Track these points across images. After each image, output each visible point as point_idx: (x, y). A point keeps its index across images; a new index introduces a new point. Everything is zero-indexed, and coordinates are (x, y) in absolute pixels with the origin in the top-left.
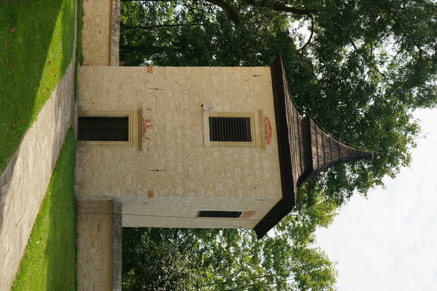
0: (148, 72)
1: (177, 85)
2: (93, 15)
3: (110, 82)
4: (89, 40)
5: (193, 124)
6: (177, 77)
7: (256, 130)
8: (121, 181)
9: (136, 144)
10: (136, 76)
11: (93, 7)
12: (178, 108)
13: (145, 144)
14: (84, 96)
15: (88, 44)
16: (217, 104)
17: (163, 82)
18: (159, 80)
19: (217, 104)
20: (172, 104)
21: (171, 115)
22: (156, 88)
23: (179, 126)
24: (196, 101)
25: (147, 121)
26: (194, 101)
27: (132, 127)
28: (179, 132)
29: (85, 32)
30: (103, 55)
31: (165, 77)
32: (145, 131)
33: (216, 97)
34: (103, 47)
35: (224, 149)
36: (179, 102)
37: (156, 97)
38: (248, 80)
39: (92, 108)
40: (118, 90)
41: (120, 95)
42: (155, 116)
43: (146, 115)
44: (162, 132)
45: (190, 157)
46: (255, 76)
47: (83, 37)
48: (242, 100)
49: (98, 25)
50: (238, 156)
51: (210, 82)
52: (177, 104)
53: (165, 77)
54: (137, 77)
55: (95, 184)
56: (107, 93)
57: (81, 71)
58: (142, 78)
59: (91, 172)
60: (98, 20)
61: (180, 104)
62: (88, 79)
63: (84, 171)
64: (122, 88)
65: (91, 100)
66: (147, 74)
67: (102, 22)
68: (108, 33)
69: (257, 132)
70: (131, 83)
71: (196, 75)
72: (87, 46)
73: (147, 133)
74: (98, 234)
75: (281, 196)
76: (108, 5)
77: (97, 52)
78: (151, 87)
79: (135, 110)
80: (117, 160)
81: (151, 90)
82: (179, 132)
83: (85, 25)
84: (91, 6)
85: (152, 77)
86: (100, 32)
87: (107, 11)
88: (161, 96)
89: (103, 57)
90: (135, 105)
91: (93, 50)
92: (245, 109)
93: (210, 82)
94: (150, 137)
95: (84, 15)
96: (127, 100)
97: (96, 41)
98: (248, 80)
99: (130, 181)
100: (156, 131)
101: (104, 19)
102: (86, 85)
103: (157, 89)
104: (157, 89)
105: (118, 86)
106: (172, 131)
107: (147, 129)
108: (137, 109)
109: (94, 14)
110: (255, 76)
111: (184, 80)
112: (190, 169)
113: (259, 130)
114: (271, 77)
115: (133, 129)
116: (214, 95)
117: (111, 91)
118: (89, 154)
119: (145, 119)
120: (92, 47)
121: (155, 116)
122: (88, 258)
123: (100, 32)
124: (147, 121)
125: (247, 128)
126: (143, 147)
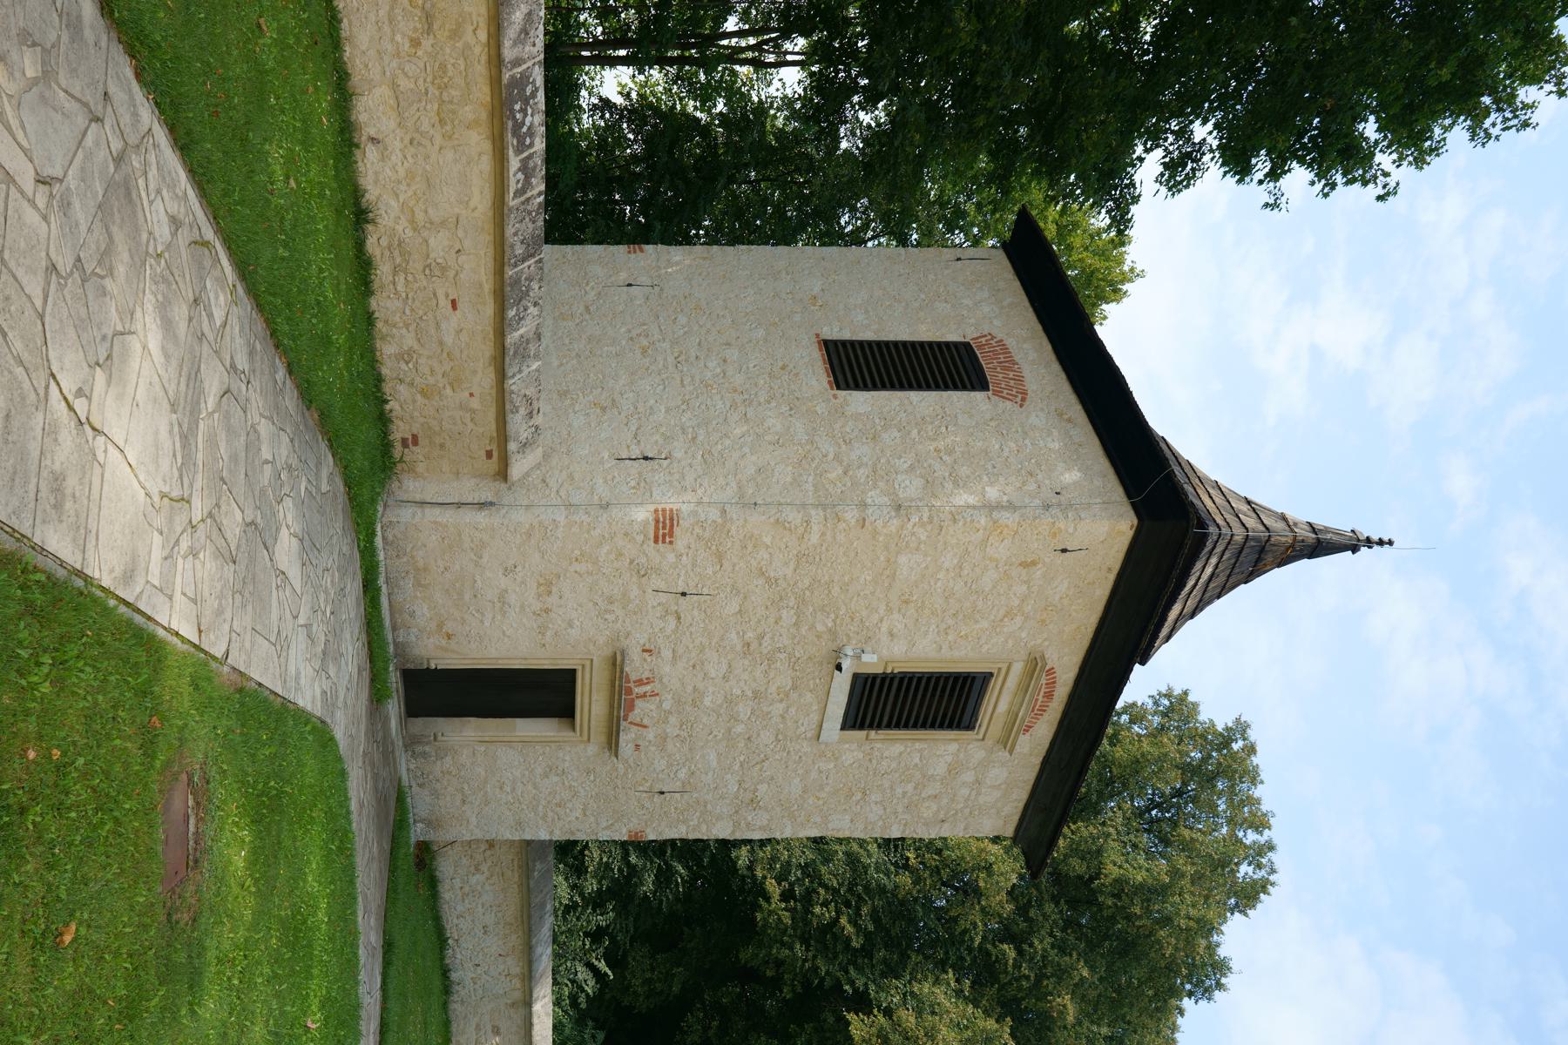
0: (656, 541)
1: (761, 581)
2: (412, 221)
3: (506, 572)
4: (409, 341)
5: (794, 687)
6: (766, 556)
7: (997, 705)
8: (550, 814)
9: (598, 736)
10: (609, 552)
11: (410, 176)
12: (754, 646)
13: (626, 738)
14: (412, 614)
15: (406, 356)
16: (891, 634)
17: (710, 571)
18: (694, 565)
19: (891, 634)
20: (734, 636)
21: (725, 667)
22: (680, 590)
23: (749, 693)
24: (820, 628)
25: (640, 682)
26: (812, 627)
27: (586, 701)
28: (744, 710)
29: (384, 304)
30: (475, 403)
31: (720, 557)
32: (631, 707)
33: (896, 616)
34: (475, 372)
35: (879, 745)
36: (759, 630)
37: (679, 618)
38: (1034, 563)
39: (446, 650)
40: (540, 595)
41: (547, 611)
42: (667, 669)
43: (636, 667)
44: (688, 708)
45: (766, 764)
46: (1064, 551)
47: (379, 325)
48: (985, 624)
49: (444, 269)
50: (917, 760)
51: (887, 572)
52: (750, 634)
53: (720, 557)
54: (612, 557)
55: (473, 820)
56: (498, 605)
57: (390, 538)
58: (632, 562)
59: (459, 797)
60: (439, 244)
61: (761, 637)
62: (421, 564)
63: (436, 794)
64: (554, 590)
65: (440, 626)
66: (650, 546)
67: (462, 258)
68: (489, 309)
69: (1003, 707)
70: (590, 574)
71: (842, 550)
72: (404, 366)
73: (636, 711)
74: (488, 853)
75: (1136, 522)
76: (486, 164)
77: (448, 391)
78: (663, 586)
79: (600, 655)
80: (539, 770)
81: (663, 598)
82: (744, 710)
83: (383, 271)
84: (402, 172)
85: (671, 557)
86: (454, 303)
87: (481, 201)
88: (696, 612)
89: (473, 411)
90: (601, 640)
91: (431, 381)
92: (986, 647)
93: (887, 572)
94: (645, 722)
95: (373, 221)
96: (570, 625)
97: (441, 343)
98: (1034, 563)
99: (578, 813)
100: (666, 706)
101: (467, 243)
102: (418, 584)
103: (684, 594)
104: (684, 594)
105: (540, 585)
106: (720, 706)
107: (639, 703)
108: (608, 652)
109: (420, 217)
110: (1064, 551)
111: (792, 566)
112: (763, 788)
113: (1011, 704)
114: (1121, 556)
115: (591, 700)
116: (889, 610)
117: (512, 599)
118: (448, 759)
119: (633, 677)
120: (427, 370)
121: (667, 669)
122: (467, 889)
123: (454, 303)
124: (640, 682)
125: (974, 695)
126: (622, 743)
